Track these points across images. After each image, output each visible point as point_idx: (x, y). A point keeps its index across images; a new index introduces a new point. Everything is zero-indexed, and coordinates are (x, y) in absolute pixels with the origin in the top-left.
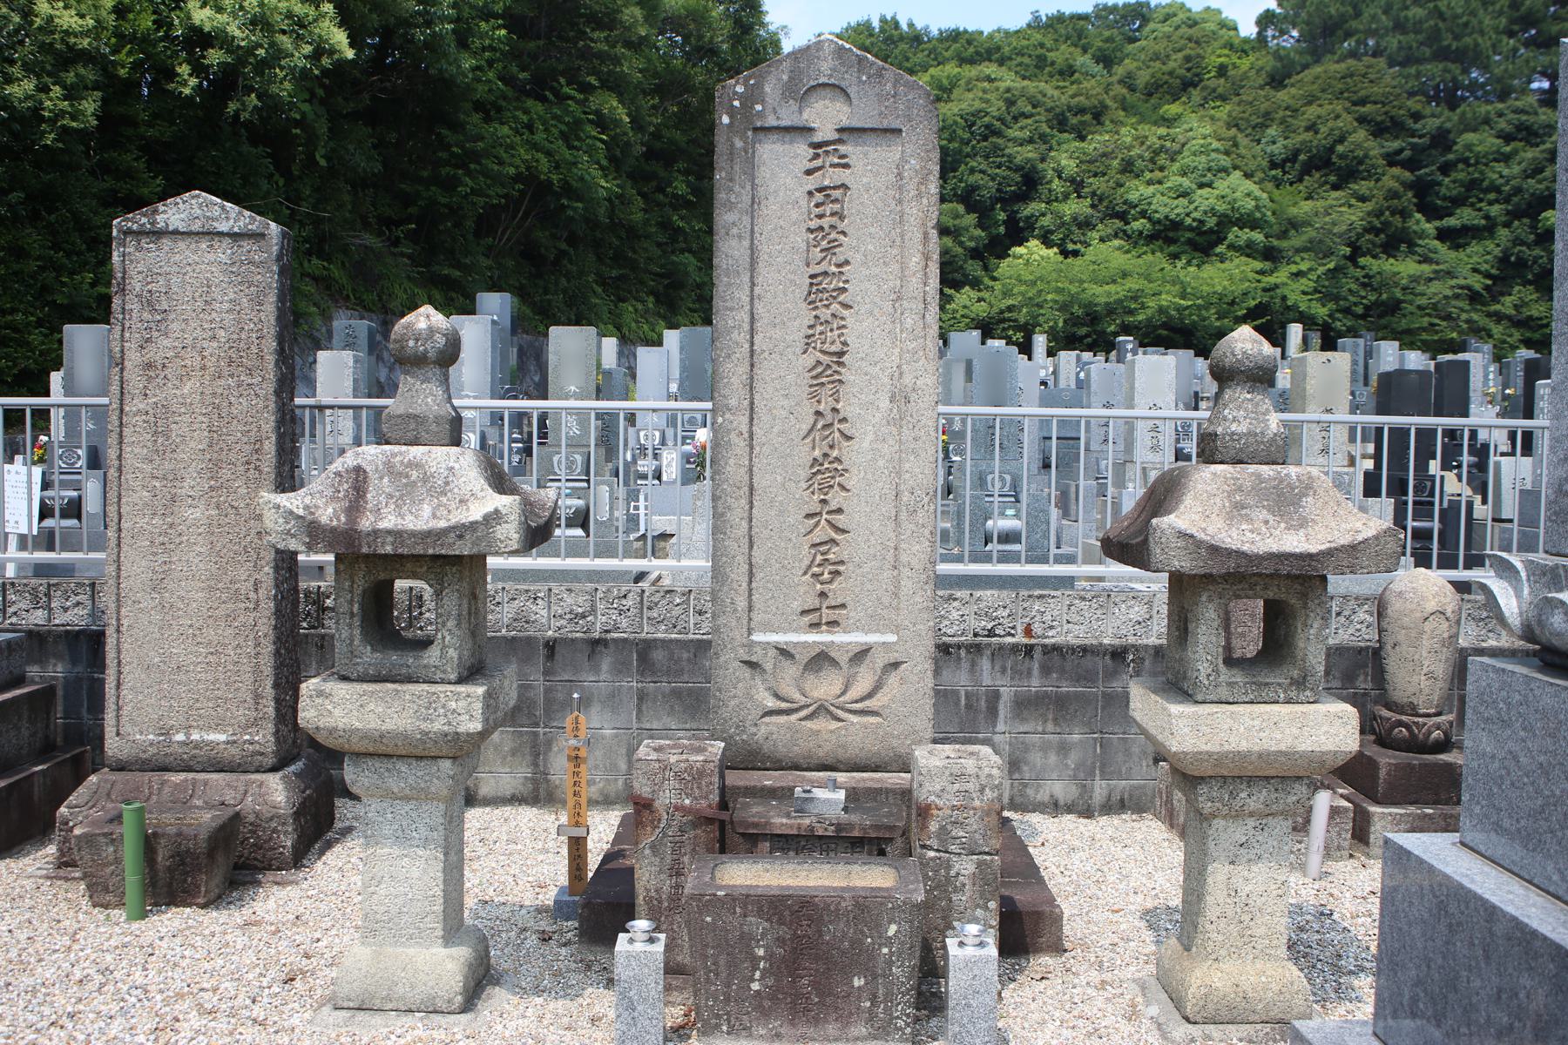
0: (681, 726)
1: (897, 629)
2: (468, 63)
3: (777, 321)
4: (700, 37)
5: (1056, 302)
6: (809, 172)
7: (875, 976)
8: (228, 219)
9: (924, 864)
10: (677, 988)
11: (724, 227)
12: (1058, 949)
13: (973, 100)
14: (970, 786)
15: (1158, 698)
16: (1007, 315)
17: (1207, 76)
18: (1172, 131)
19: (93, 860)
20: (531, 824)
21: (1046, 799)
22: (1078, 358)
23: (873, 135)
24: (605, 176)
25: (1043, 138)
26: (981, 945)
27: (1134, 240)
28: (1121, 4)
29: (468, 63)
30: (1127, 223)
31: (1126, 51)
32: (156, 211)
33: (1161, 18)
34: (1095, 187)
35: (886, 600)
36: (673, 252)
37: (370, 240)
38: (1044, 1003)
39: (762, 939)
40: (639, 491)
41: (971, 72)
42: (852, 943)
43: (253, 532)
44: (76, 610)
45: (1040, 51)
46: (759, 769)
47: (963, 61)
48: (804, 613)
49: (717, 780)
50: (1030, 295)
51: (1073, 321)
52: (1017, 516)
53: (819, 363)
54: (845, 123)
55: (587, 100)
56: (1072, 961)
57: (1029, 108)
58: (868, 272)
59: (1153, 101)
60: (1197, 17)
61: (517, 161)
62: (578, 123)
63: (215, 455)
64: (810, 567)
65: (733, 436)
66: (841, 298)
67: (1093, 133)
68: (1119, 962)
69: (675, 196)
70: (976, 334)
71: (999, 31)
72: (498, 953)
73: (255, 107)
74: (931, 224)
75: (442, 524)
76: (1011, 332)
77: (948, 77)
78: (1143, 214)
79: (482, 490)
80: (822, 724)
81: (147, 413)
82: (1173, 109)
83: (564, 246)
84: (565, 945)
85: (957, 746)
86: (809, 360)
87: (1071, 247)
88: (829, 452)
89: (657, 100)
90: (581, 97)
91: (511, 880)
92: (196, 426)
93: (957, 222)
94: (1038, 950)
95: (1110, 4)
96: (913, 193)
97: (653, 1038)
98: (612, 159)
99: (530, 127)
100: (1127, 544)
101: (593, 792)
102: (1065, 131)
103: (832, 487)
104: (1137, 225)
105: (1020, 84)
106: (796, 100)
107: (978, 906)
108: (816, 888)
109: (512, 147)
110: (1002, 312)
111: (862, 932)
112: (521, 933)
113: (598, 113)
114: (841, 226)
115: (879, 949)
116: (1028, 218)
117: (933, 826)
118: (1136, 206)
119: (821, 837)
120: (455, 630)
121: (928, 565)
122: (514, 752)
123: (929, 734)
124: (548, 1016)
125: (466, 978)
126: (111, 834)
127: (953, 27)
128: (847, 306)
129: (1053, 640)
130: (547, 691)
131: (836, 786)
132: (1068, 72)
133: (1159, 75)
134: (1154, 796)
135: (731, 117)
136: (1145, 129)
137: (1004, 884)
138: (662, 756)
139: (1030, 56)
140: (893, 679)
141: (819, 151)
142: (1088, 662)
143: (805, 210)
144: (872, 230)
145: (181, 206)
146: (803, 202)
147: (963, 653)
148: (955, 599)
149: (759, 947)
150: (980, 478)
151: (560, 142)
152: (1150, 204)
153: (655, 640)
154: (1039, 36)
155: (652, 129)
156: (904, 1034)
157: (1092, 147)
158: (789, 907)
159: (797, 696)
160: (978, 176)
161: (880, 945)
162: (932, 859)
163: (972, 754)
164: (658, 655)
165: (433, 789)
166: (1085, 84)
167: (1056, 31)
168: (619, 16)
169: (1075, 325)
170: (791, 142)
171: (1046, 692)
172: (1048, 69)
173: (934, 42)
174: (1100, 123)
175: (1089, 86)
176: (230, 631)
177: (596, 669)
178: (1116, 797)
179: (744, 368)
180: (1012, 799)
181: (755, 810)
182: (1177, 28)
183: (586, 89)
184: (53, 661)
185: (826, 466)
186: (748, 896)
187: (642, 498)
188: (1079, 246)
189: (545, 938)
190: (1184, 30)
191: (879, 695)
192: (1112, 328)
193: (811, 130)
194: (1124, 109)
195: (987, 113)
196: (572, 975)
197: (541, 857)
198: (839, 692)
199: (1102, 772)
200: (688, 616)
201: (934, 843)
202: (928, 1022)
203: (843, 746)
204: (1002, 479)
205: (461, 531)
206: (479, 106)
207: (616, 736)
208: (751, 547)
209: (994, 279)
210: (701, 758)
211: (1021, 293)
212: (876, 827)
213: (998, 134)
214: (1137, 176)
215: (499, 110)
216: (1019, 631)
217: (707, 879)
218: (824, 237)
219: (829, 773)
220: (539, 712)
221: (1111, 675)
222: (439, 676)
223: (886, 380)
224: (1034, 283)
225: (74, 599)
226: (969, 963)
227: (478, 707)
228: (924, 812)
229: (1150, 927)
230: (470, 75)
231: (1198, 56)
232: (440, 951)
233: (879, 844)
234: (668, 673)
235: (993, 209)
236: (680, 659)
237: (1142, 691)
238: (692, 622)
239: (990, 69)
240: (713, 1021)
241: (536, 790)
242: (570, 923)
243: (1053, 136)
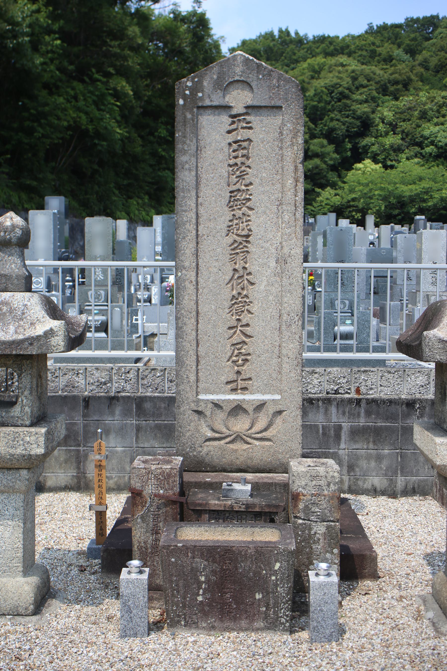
0: (161, 446)
1: (280, 392)
2: (38, 60)
3: (211, 218)
4: (174, 44)
5: (380, 195)
6: (229, 132)
7: (268, 593)
9: (296, 527)
10: (156, 599)
11: (181, 164)
12: (375, 576)
13: (333, 78)
14: (322, 483)
15: (429, 434)
16: (352, 203)
20: (76, 503)
21: (370, 487)
22: (392, 229)
23: (266, 110)
24: (119, 127)
25: (374, 99)
26: (329, 575)
29: (38, 60)
30: (423, 148)
31: (423, 46)
34: (403, 128)
35: (274, 376)
36: (159, 170)
38: (367, 609)
39: (203, 571)
40: (138, 310)
41: (332, 61)
42: (255, 574)
45: (373, 47)
46: (203, 472)
47: (327, 54)
48: (228, 383)
49: (178, 479)
50: (365, 191)
51: (390, 206)
52: (352, 324)
53: (235, 241)
54: (250, 103)
55: (108, 82)
56: (383, 584)
57: (366, 82)
58: (263, 189)
61: (69, 118)
62: (102, 97)
64: (231, 357)
65: (187, 283)
66: (248, 204)
67: (403, 96)
68: (410, 585)
69: (160, 137)
70: (333, 216)
71: (348, 36)
72: (56, 579)
74: (298, 161)
75: (21, 337)
76: (354, 213)
77: (318, 64)
78: (432, 143)
79: (43, 317)
80: (239, 446)
83: (96, 167)
84: (93, 573)
85: (315, 459)
86: (229, 240)
87: (389, 163)
88: (241, 292)
89: (149, 81)
90: (105, 80)
91: (63, 536)
93: (323, 150)
94: (363, 577)
95: (415, 18)
96: (289, 143)
97: (142, 629)
98: (123, 116)
99: (75, 98)
100: (410, 345)
101: (111, 483)
102: (387, 95)
103: (243, 311)
104: (428, 150)
106: (221, 90)
107: (327, 551)
108: (233, 542)
109: (65, 110)
110: (349, 202)
111: (260, 567)
112: (68, 567)
113: (115, 89)
114: (248, 163)
115: (270, 577)
116: (364, 147)
117: (301, 506)
118: (428, 138)
119: (237, 512)
120: (29, 396)
121: (298, 356)
122: (66, 461)
123: (299, 452)
124: (83, 616)
125: (36, 595)
127: (321, 34)
128: (251, 209)
129: (372, 396)
130: (85, 426)
131: (246, 482)
132: (389, 59)
133: (442, 60)
134: (432, 487)
135: (184, 100)
136: (434, 93)
137: (343, 538)
138: (147, 466)
139: (366, 50)
140: (279, 420)
141: (235, 120)
142: (393, 408)
143: (227, 154)
144: (265, 165)
146: (226, 150)
147: (320, 403)
148: (316, 373)
149: (202, 576)
150: (331, 303)
151: (93, 107)
152: (436, 137)
153: (146, 397)
154: (372, 39)
155: (146, 98)
156: (285, 626)
157: (402, 104)
158: (219, 553)
159: (224, 430)
160: (335, 123)
161: (271, 575)
162: (301, 524)
163: (323, 464)
164: (147, 405)
165: (17, 487)
166: (399, 67)
167: (382, 35)
168: (126, 32)
169: (391, 208)
170: (219, 115)
171: (368, 426)
172: (377, 58)
173: (310, 44)
174: (408, 90)
177: (112, 413)
178: (410, 486)
179: (192, 245)
180: (349, 487)
181: (200, 496)
183: (108, 75)
185: (240, 300)
186: (195, 546)
187: (139, 314)
188: (394, 163)
189: (82, 570)
191: (271, 429)
192: (413, 210)
193: (230, 107)
194: (422, 81)
195: (341, 86)
196: (97, 592)
197: (81, 522)
198: (248, 428)
199: (402, 472)
200: (164, 383)
201: (301, 515)
202: (299, 619)
203: (251, 459)
204: (343, 303)
205: (32, 341)
206: (46, 86)
207: (124, 451)
208: (198, 346)
209: (344, 182)
210: (169, 467)
211: (361, 191)
212: (268, 506)
214: (429, 121)
215: (57, 88)
216: (353, 391)
217: (172, 536)
218: (238, 170)
219: (243, 474)
221: (406, 416)
222: (20, 422)
223: (274, 251)
224: (367, 185)
226: (321, 586)
227: (42, 440)
228: (296, 497)
229: (429, 564)
230: (40, 68)
232: (21, 580)
233: (270, 516)
234: (153, 415)
235: (344, 142)
236: (160, 407)
237: (420, 429)
238: (166, 386)
239: (343, 59)
240: (176, 619)
241: (79, 482)
242: (96, 561)
243: (379, 98)
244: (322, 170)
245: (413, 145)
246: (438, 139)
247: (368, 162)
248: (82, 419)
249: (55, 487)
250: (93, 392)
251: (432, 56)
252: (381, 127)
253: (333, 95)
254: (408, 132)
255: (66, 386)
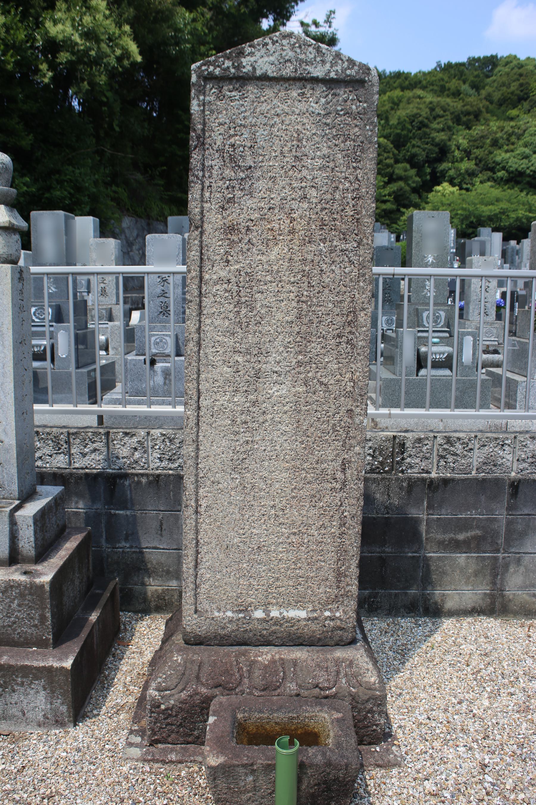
8: (323, 62)
13: (413, 108)
17: (531, 94)
18: (518, 123)
19: (230, 788)
25: (449, 128)
27: (499, 182)
28: (482, 57)
30: (494, 173)
32: (241, 53)
33: (504, 64)
34: (477, 154)
37: (139, 176)
41: (409, 94)
43: (343, 409)
44: (93, 456)
45: (442, 83)
57: (442, 112)
59: (503, 108)
60: (523, 63)
63: (304, 328)
71: (420, 72)
73: (87, 90)
77: (397, 97)
81: (229, 281)
82: (514, 112)
87: (465, 186)
92: (283, 296)
93: (406, 173)
95: (476, 57)
104: (500, 174)
105: (435, 100)
116: (442, 171)
118: (500, 164)
122: (476, 574)
126: (252, 765)
127: (397, 70)
130: (509, 523)
132: (457, 94)
133: (506, 94)
145: (270, 46)
152: (507, 163)
172: (446, 93)
175: (472, 100)
176: (313, 511)
182: (512, 69)
184: (75, 499)
188: (469, 186)
190: (516, 70)
195: (420, 116)
213: (426, 126)
214: (500, 148)
220: (501, 541)
225: (91, 446)
231: (527, 83)
241: (493, 603)
243: (454, 128)
244: (405, 192)
245: (486, 170)
246: (509, 164)
247: (445, 184)
248: (505, 513)
249: (457, 610)
250: (524, 472)
251: (494, 91)
252: (457, 153)
253: (413, 123)
254: (482, 158)
255: (485, 463)
